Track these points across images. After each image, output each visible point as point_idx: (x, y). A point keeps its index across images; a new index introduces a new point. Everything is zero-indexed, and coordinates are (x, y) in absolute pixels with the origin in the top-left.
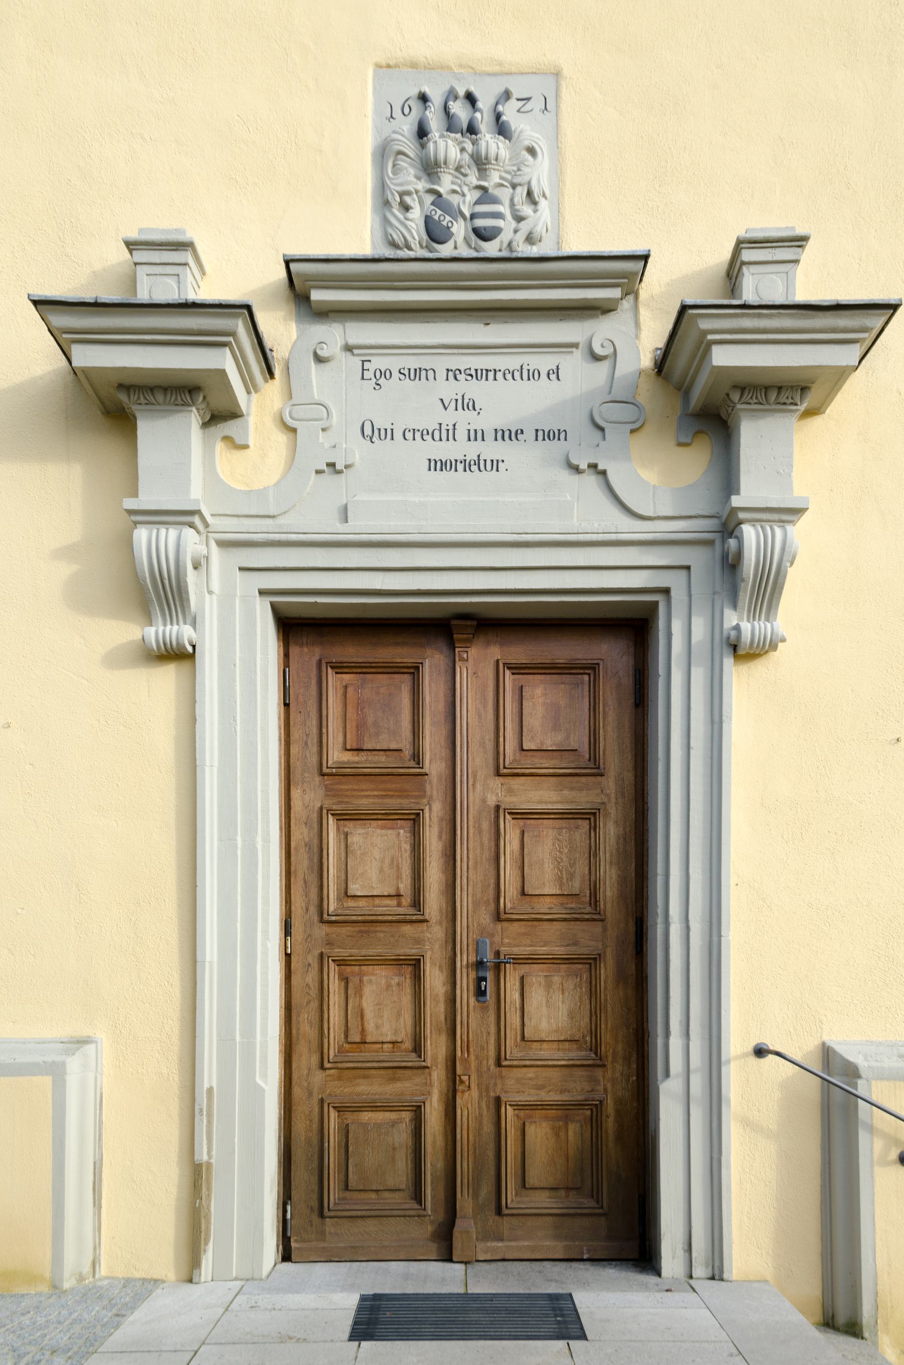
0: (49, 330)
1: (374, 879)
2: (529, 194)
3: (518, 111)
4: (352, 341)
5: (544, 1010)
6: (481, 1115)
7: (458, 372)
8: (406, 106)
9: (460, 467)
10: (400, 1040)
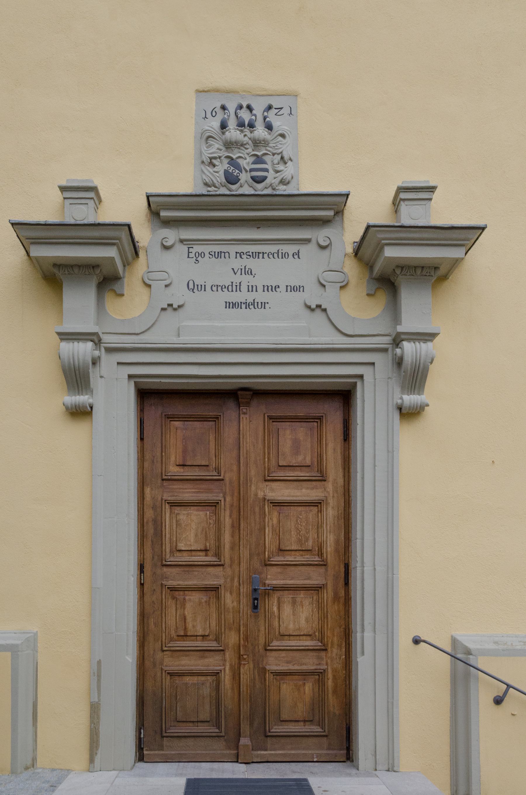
0: (17, 236)
1: (192, 541)
2: (282, 158)
3: (276, 115)
4: (183, 237)
5: (292, 617)
6: (255, 679)
7: (242, 254)
8: (214, 111)
9: (243, 306)
10: (207, 634)
